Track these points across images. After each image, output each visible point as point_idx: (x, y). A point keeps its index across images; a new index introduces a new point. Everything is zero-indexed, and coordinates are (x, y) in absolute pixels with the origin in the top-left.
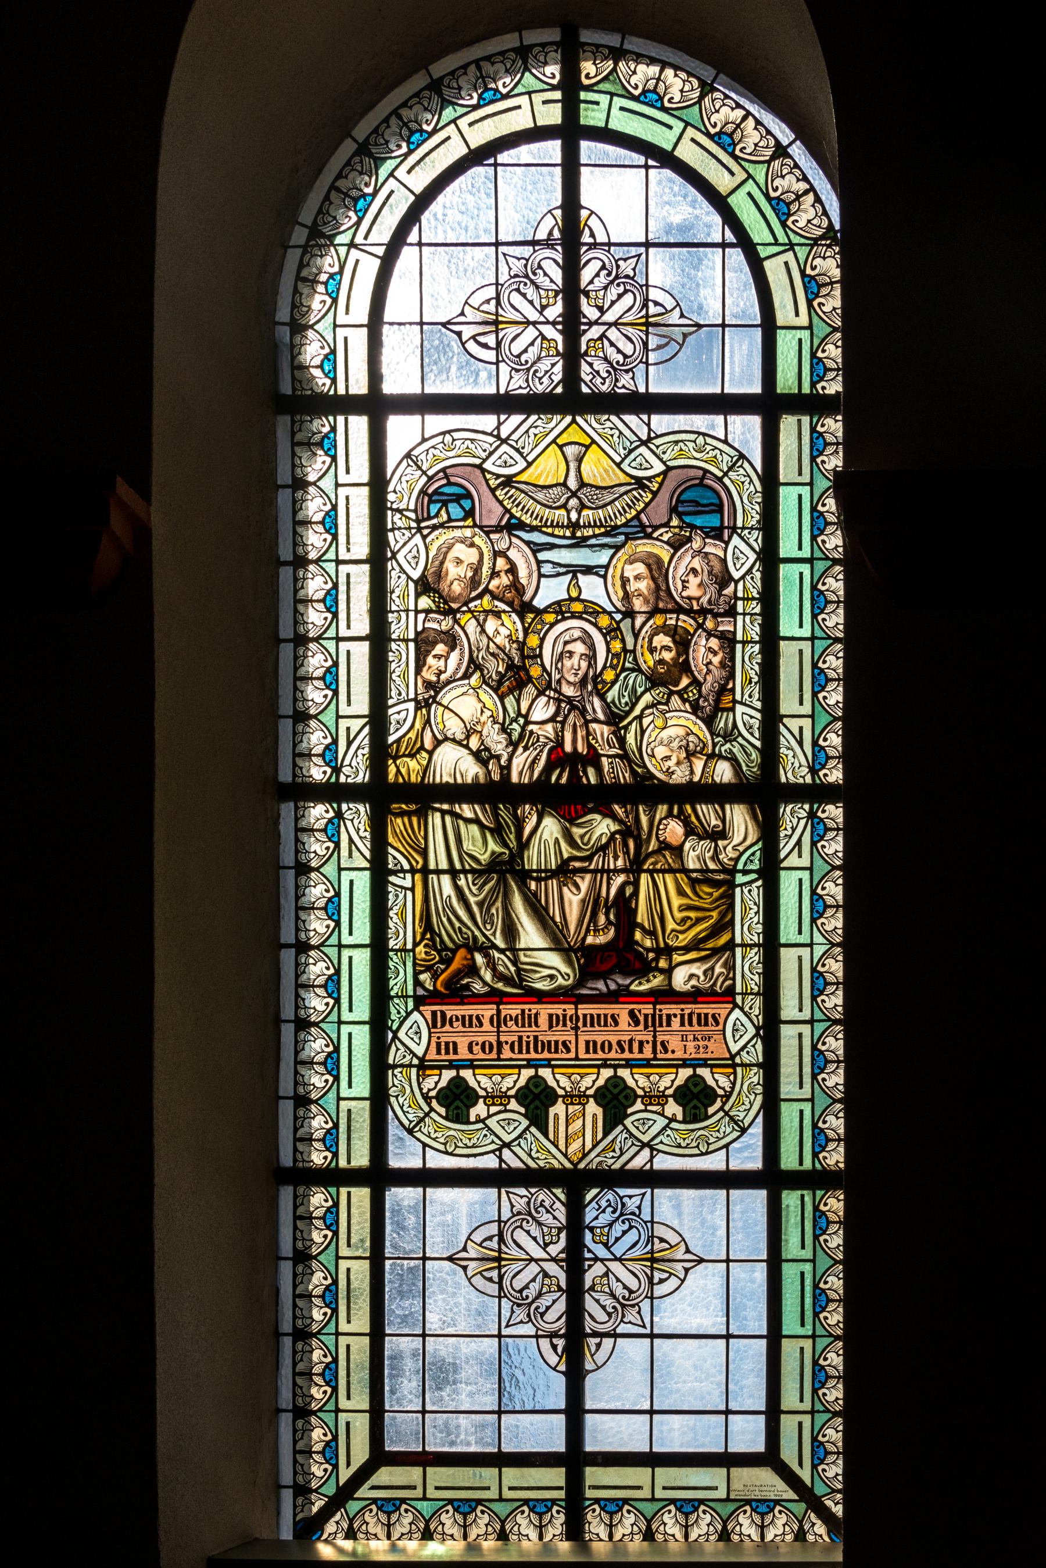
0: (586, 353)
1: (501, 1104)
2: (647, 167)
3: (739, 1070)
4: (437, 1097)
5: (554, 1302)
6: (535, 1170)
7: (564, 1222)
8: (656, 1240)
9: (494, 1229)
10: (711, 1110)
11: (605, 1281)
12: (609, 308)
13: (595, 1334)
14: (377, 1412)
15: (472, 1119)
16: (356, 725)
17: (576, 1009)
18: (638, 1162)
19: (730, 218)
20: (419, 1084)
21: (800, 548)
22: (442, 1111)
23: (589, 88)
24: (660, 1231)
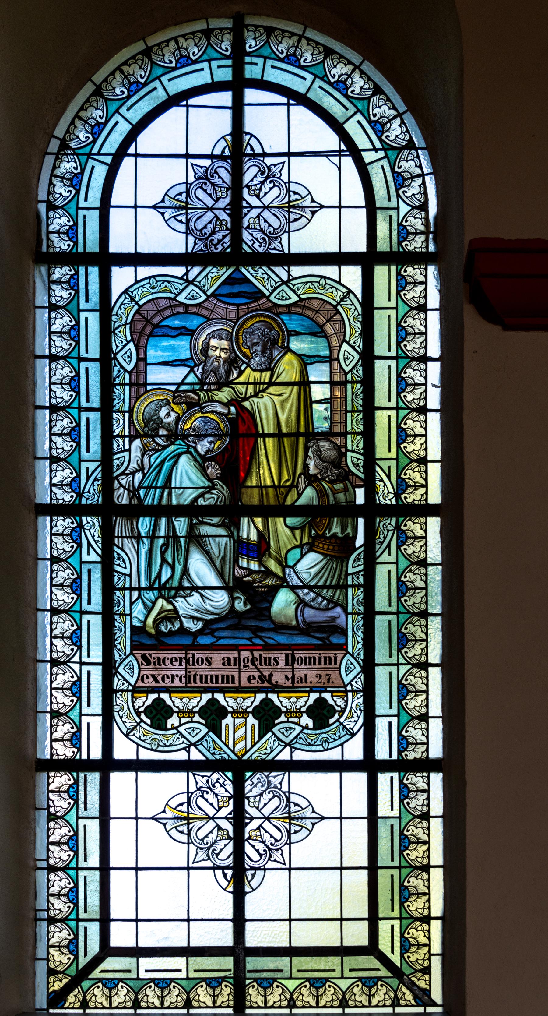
0: (230, 798)
1: (189, 717)
2: (288, 105)
3: (350, 694)
4: (145, 712)
5: (226, 845)
6: (264, 265)
7: (232, 792)
8: (292, 805)
9: (184, 798)
10: (331, 721)
11: (219, 195)
12: (214, 827)
13: (252, 868)
14: (105, 920)
15: (169, 726)
16: (385, 557)
17: (239, 654)
18: (195, 270)
19: (344, 136)
20: (133, 703)
21: (389, 351)
22: (149, 722)
23: (249, 54)
24: (293, 187)
